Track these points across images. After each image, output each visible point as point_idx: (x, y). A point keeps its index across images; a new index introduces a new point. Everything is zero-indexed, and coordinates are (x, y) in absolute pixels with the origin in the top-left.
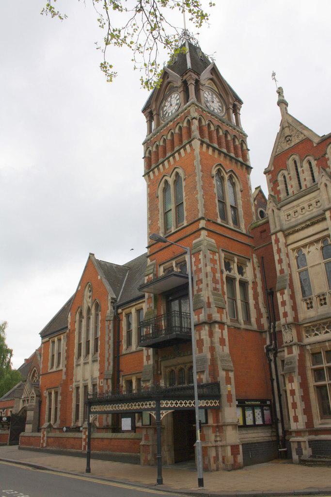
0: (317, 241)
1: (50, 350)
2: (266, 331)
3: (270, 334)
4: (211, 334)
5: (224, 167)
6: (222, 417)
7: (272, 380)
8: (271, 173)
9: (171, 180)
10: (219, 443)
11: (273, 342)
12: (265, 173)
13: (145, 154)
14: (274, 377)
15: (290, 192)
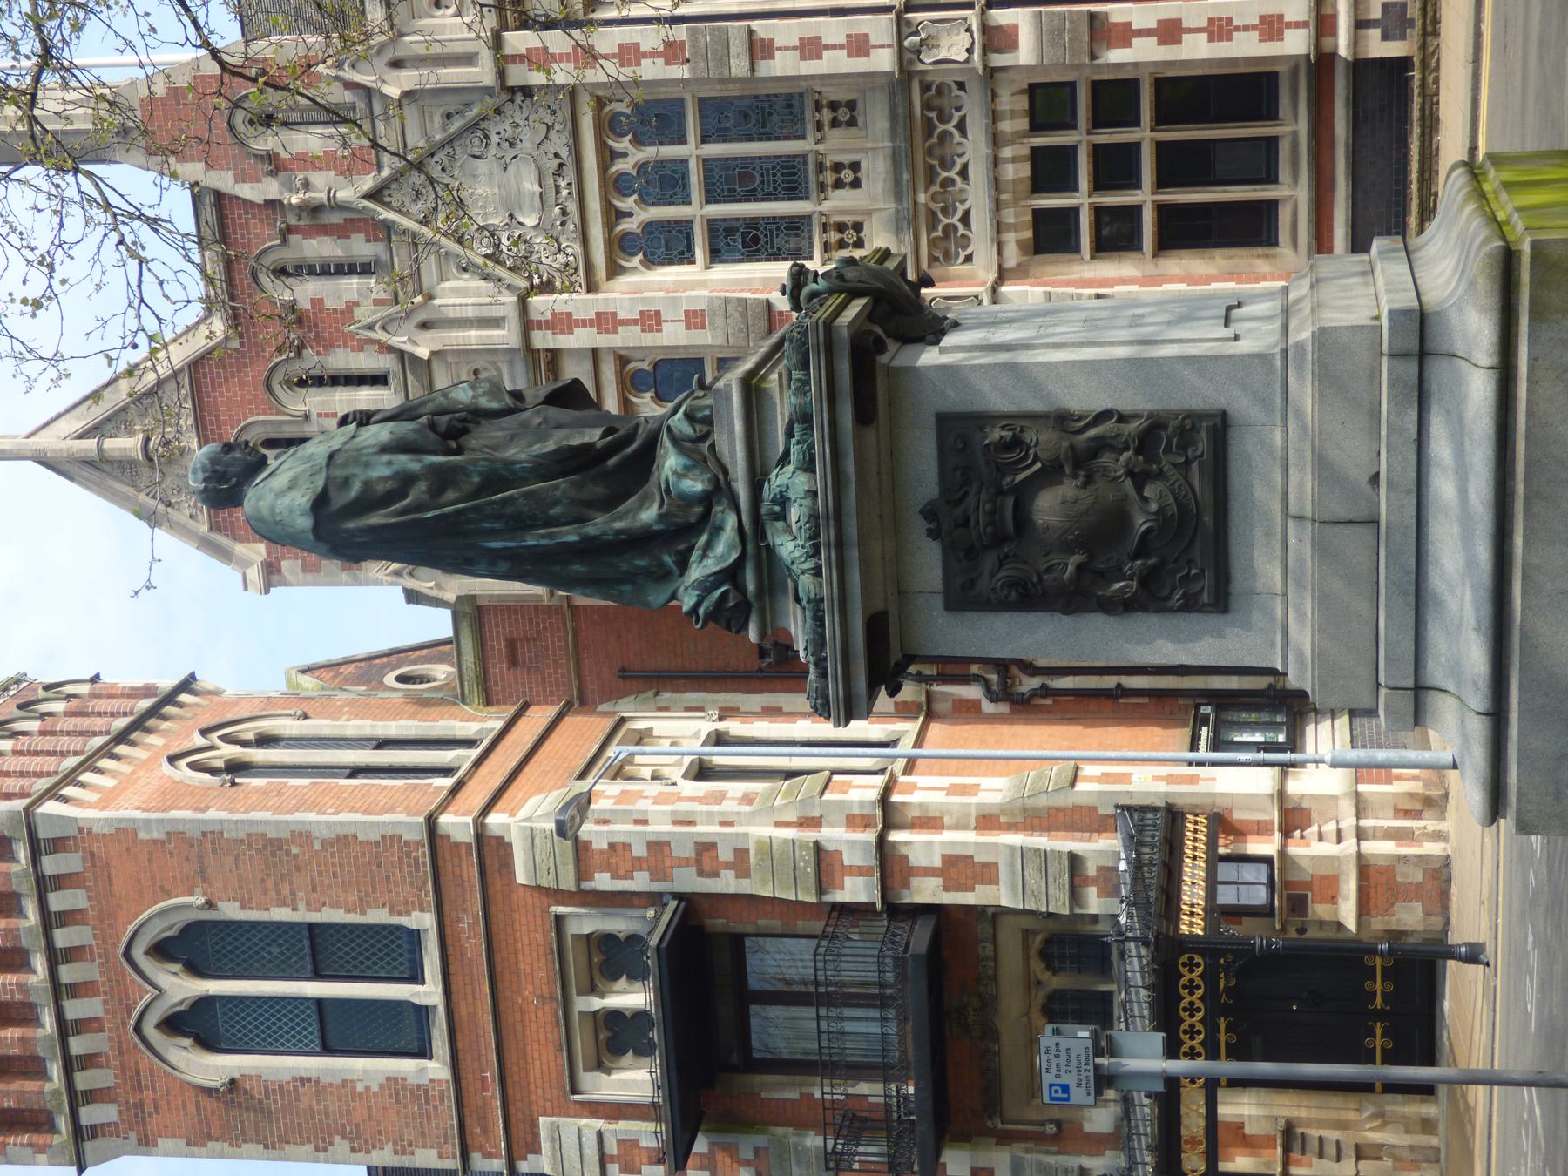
1: (855, 578)
2: (928, 695)
3: (944, 678)
4: (930, 822)
5: (229, 717)
7: (1122, 692)
9: (181, 987)
10: (1348, 822)
11: (975, 669)
12: (267, 592)
14: (1109, 682)
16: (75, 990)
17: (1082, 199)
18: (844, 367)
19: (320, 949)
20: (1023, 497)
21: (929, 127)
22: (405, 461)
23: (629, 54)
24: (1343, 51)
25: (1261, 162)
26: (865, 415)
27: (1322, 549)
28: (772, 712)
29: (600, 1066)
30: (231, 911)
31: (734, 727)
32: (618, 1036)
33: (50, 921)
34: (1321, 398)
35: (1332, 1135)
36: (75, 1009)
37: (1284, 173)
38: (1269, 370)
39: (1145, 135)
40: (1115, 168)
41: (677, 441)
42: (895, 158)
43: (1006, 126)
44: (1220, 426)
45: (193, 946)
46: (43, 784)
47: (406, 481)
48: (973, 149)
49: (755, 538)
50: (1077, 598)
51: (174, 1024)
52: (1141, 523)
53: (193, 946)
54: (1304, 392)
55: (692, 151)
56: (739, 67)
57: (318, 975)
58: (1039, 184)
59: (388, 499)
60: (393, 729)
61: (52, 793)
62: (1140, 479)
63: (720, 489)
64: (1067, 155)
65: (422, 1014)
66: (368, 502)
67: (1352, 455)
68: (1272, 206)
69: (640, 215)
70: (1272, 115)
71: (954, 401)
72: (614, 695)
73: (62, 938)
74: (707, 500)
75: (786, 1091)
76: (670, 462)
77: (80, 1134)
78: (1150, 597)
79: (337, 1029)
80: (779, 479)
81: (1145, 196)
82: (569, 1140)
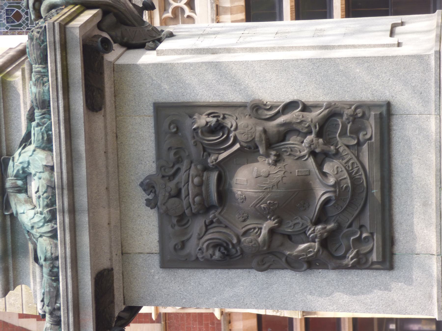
1: (85, 239)
18: (77, 62)
20: (224, 172)
52: (321, 194)
62: (320, 157)
71: (169, 94)
78: (329, 255)
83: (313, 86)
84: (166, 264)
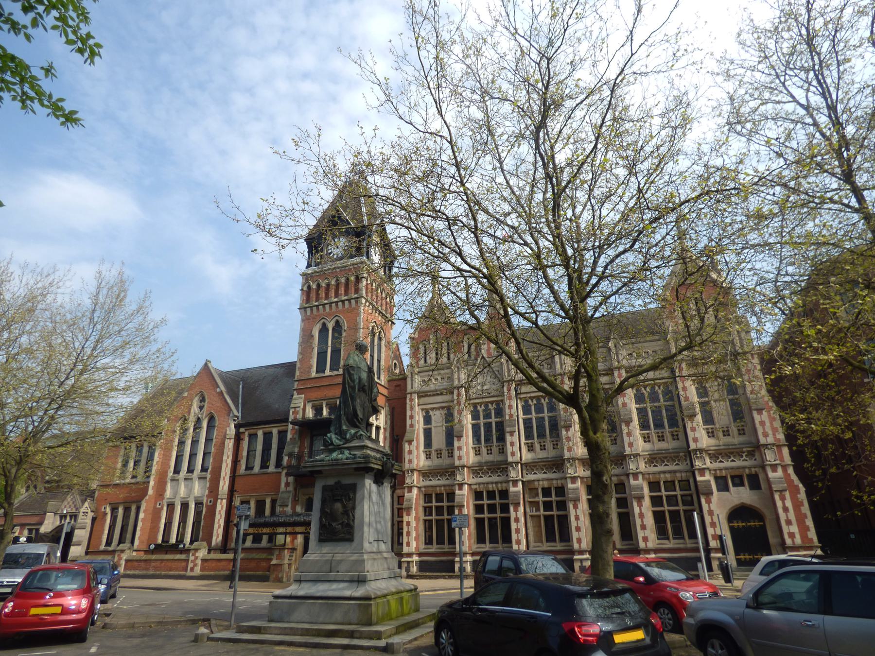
0: (443, 408)
1: (327, 468)
6: (253, 649)
8: (414, 354)
9: (330, 326)
13: (303, 286)
14: (356, 642)
15: (429, 361)
16: (331, 306)
17: (485, 502)
18: (362, 465)
19: (336, 352)
20: (340, 501)
21: (499, 469)
22: (357, 381)
23: (510, 407)
24: (575, 557)
25: (494, 540)
26: (356, 469)
27: (327, 561)
28: (385, 438)
29: (313, 406)
30: (344, 334)
31: (382, 431)
32: (318, 410)
33: (343, 301)
34: (353, 561)
35: (293, 558)
36: (327, 307)
37: (549, 544)
38: (360, 550)
39: (498, 515)
40: (492, 508)
41: (356, 433)
42: (493, 462)
43: (499, 485)
44: (350, 540)
45: (338, 326)
46: (369, 299)
47: (353, 381)
48: (495, 478)
49: (339, 448)
50: (323, 511)
51: (324, 325)
52: (334, 524)
53: (338, 326)
54: (355, 557)
55: (493, 420)
56: (508, 429)
57: (332, 351)
58: (488, 492)
59: (351, 379)
60: (382, 363)
61: (367, 300)
62: (342, 524)
63: (347, 441)
64: (494, 498)
65: (324, 372)
66: (350, 375)
67: (343, 567)
68: (485, 543)
69: (481, 409)
70: (547, 541)
71: (358, 486)
72: (390, 406)
73: (340, 304)
74: (345, 438)
75: (307, 443)
76: (353, 431)
77: (305, 308)
78: (322, 526)
79: (322, 355)
80: (347, 452)
81: (486, 515)
82: (300, 401)
83: (835, 224)
84: (324, 486)
